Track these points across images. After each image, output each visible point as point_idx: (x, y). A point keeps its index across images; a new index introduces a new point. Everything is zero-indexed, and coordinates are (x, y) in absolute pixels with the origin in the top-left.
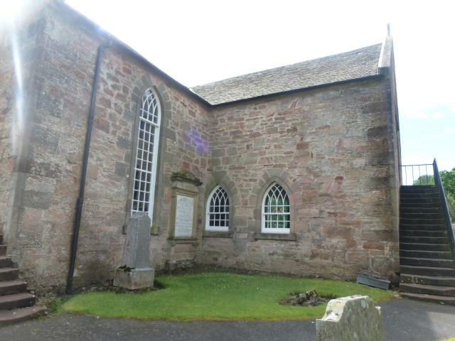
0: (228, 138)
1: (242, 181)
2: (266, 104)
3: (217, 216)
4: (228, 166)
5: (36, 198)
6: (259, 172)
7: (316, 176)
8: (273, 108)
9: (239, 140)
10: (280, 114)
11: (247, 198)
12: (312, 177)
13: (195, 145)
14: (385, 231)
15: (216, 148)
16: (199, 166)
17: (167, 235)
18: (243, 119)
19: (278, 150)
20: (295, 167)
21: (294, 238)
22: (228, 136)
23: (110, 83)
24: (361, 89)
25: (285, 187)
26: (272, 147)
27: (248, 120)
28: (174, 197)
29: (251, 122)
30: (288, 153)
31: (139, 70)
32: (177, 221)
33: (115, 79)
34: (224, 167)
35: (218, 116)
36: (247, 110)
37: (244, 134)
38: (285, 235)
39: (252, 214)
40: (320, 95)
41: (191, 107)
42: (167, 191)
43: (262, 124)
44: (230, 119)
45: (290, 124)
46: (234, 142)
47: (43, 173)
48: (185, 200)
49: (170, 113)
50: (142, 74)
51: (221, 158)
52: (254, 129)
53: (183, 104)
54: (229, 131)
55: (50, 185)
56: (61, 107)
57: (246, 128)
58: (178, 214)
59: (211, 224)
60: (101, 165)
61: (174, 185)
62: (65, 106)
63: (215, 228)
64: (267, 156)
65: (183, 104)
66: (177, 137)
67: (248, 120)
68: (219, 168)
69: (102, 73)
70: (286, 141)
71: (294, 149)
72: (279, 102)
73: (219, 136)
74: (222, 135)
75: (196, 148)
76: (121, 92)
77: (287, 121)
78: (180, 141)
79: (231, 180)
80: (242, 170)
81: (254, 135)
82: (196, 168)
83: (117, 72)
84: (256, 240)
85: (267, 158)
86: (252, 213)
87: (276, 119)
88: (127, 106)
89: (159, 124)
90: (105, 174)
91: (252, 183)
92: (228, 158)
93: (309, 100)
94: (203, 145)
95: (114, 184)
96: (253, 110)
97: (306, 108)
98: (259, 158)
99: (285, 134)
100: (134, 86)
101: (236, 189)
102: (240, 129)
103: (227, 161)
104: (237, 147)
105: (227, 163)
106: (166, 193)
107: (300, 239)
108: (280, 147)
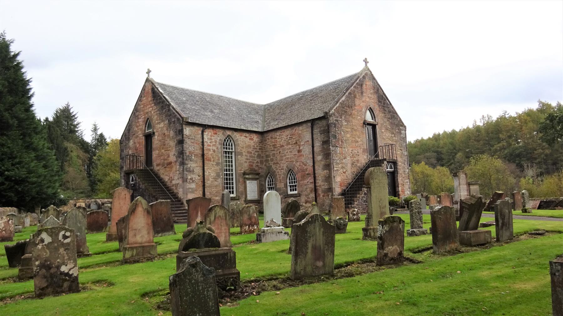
0: (271, 148)
1: (278, 170)
2: (285, 130)
3: (293, 186)
4: (272, 163)
5: (190, 190)
6: (284, 165)
7: (306, 165)
8: (288, 132)
9: (276, 149)
10: (290, 135)
11: (281, 178)
12: (304, 166)
13: (255, 154)
14: (329, 188)
15: (267, 153)
16: (259, 164)
17: (243, 199)
18: (276, 138)
19: (291, 153)
20: (298, 162)
21: (299, 195)
22: (271, 147)
23: (209, 141)
24: (319, 122)
25: (294, 171)
26: (289, 152)
27: (279, 138)
28: (245, 182)
29: (280, 140)
30: (295, 155)
31: (220, 131)
32: (248, 192)
33: (211, 139)
34: (271, 163)
35: (267, 136)
36: (278, 133)
37: (278, 146)
38: (296, 194)
39: (283, 186)
40: (304, 125)
41: (251, 136)
42: (241, 180)
43: (284, 141)
44: (272, 138)
45: (295, 140)
46: (274, 150)
47: (191, 181)
48: (251, 182)
49: (239, 144)
50: (222, 132)
51: (269, 159)
52: (281, 143)
53: (245, 136)
54: (271, 145)
55: (193, 186)
56: (193, 158)
57: (278, 143)
58: (248, 189)
59: (291, 191)
60: (210, 175)
61: (244, 177)
62: (194, 157)
63: (292, 193)
64: (287, 157)
65: (245, 136)
66: (244, 154)
67: (279, 138)
68: (270, 164)
69: (205, 139)
70: (294, 149)
71: (297, 153)
72: (290, 129)
73: (268, 147)
74: (269, 146)
75: (256, 156)
76: (214, 143)
77: (294, 139)
78: (245, 155)
79: (274, 170)
80: (278, 165)
81: (282, 146)
82: (257, 166)
83: (211, 136)
84: (286, 198)
85: (287, 158)
86: (283, 186)
87: (289, 138)
88: (217, 148)
89: (234, 150)
90: (212, 177)
91: (282, 170)
92: (272, 159)
93: (301, 128)
94: (260, 153)
95: (216, 181)
96: (280, 133)
97: (300, 132)
98: (284, 158)
99: (293, 145)
100: (219, 138)
101: (276, 174)
102: (276, 144)
103: (272, 160)
104: (275, 153)
105: (272, 161)
106: (241, 181)
107: (301, 195)
108: (292, 152)
